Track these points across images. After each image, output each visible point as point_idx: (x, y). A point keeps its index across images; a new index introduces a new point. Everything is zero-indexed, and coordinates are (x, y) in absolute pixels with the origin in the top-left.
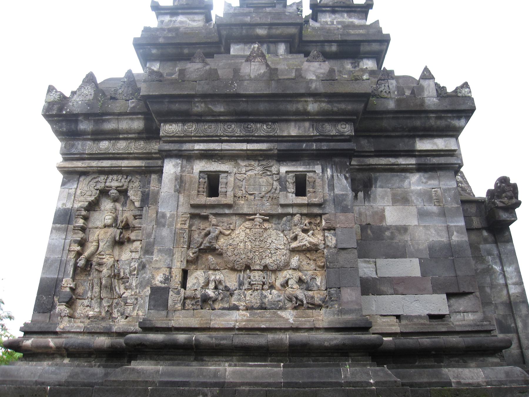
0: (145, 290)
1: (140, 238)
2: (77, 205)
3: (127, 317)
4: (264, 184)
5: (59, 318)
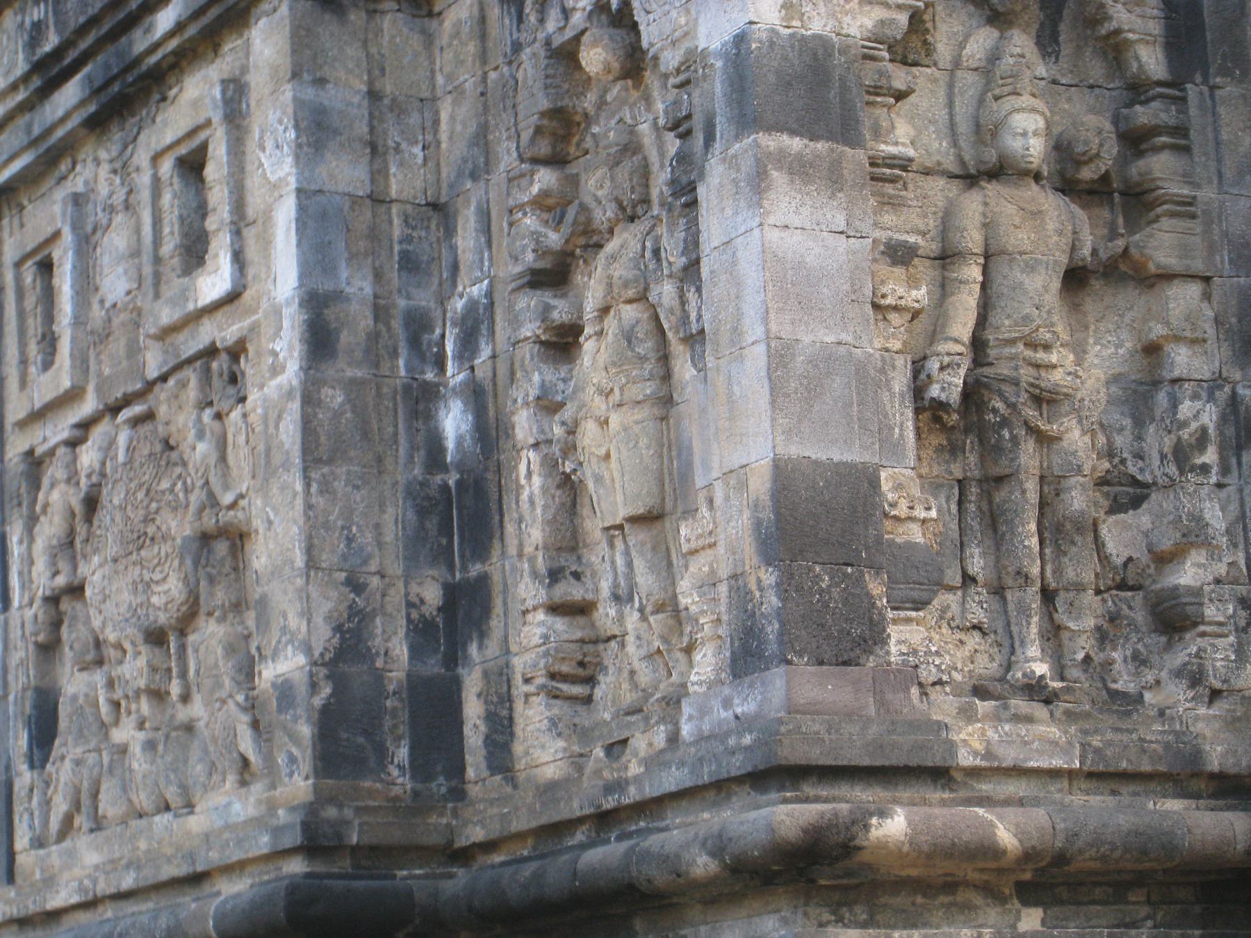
1: (1198, 266)
3: (1215, 694)
5: (915, 691)
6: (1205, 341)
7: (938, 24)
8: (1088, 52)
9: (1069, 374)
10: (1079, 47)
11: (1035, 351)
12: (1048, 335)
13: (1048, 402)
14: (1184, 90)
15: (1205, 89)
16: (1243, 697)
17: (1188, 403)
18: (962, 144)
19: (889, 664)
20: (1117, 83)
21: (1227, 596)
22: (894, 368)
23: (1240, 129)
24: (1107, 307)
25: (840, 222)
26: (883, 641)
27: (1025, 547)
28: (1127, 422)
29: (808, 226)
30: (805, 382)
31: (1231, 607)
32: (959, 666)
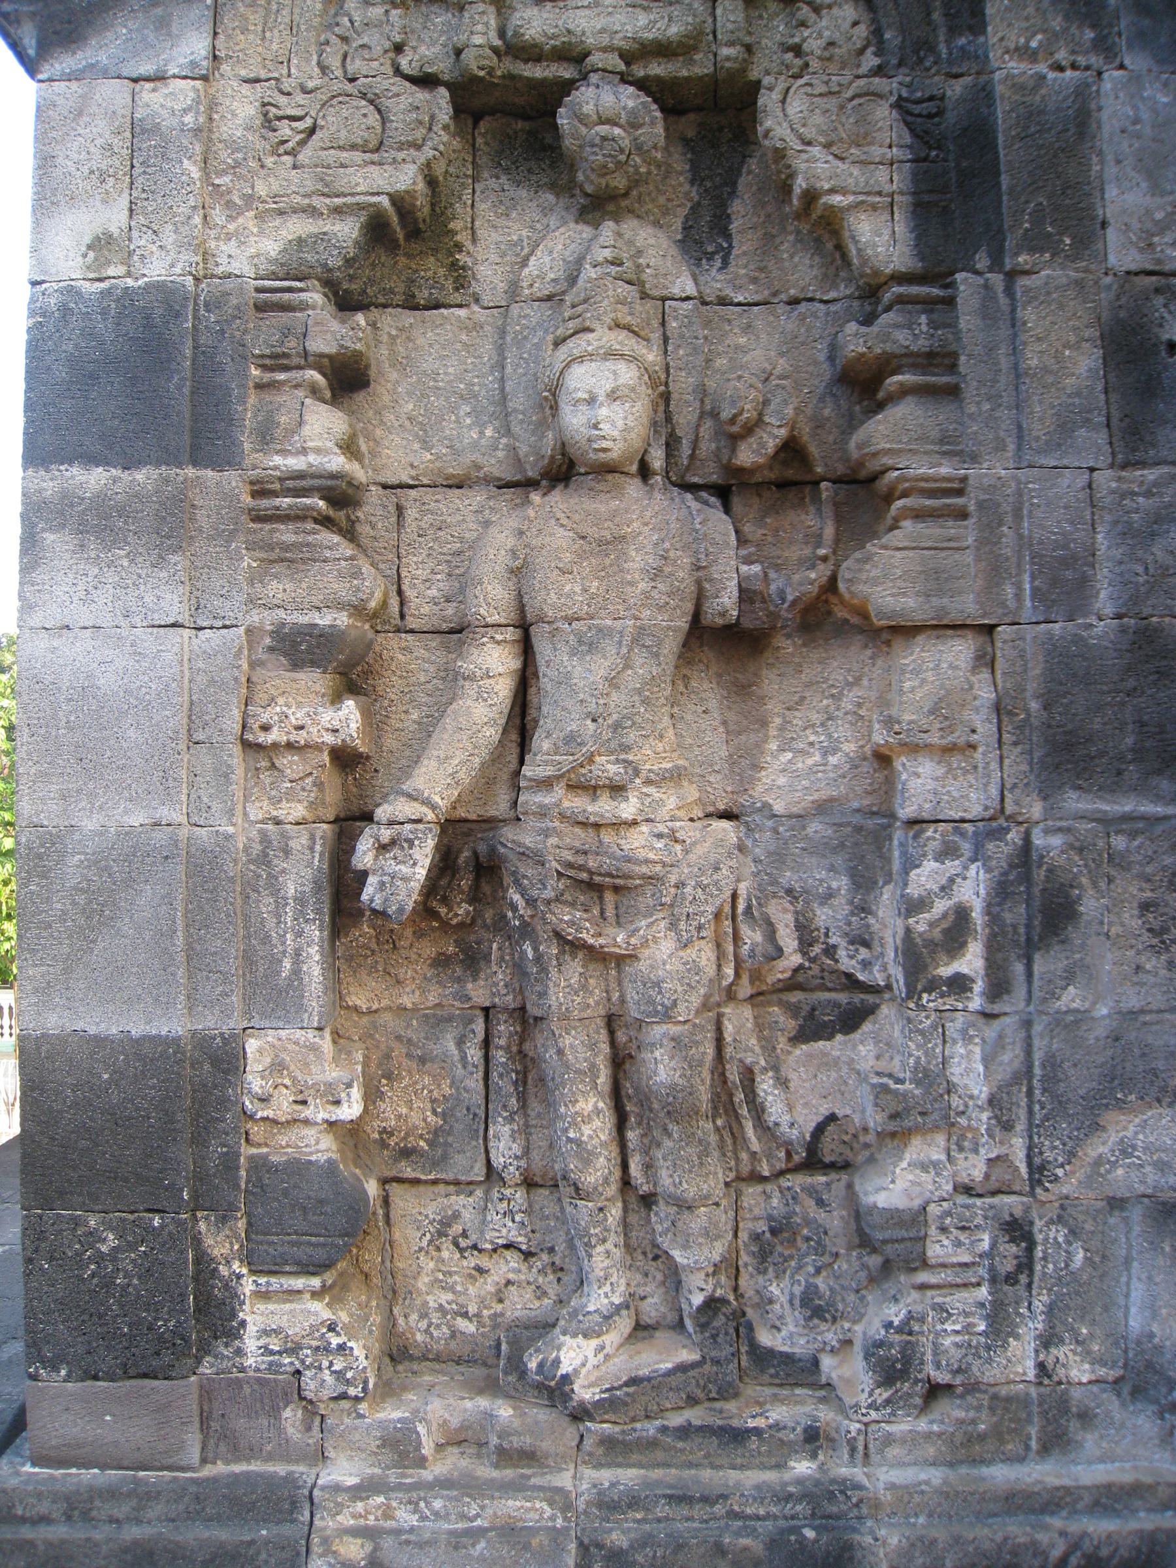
0: (1099, 1147)
1: (967, 606)
2: (249, 251)
3: (934, 1391)
5: (291, 1415)
6: (973, 747)
7: (480, 233)
8: (787, 244)
9: (660, 836)
10: (769, 237)
11: (594, 798)
12: (613, 769)
13: (616, 889)
14: (952, 285)
15: (997, 280)
16: (995, 1397)
17: (930, 865)
18: (516, 429)
19: (242, 1370)
20: (844, 290)
22: (287, 852)
23: (1066, 346)
24: (809, 685)
25: (173, 605)
26: (232, 1331)
27: (569, 1140)
28: (841, 883)
29: (106, 621)
30: (81, 899)
31: (986, 1237)
32: (472, 1309)
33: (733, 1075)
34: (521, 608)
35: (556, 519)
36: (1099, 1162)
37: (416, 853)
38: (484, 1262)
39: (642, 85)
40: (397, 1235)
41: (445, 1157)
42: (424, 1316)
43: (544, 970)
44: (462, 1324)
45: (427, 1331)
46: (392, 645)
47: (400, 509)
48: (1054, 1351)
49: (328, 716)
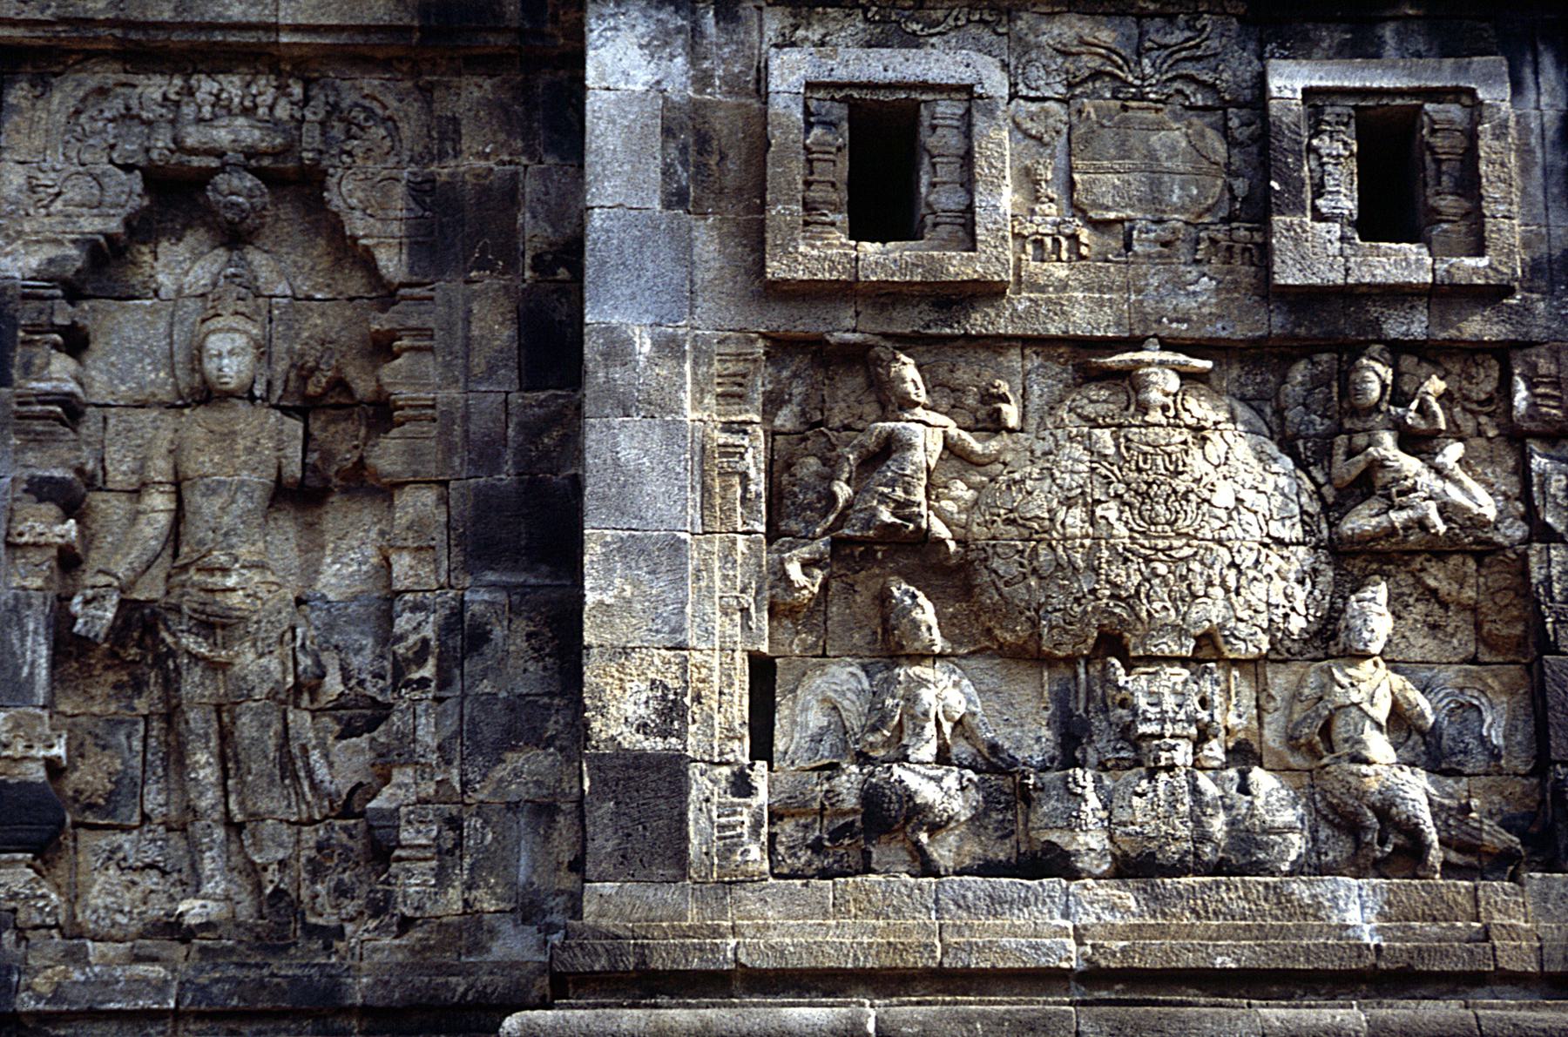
0: (499, 772)
1: (431, 470)
3: (406, 924)
4: (1177, 164)
5: (9, 937)
12: (223, 558)
13: (224, 627)
18: (178, 373)
21: (431, 817)
22: (30, 606)
23: (496, 322)
28: (368, 642)
32: (127, 909)
33: (295, 749)
34: (176, 473)
35: (198, 424)
36: (501, 780)
37: (107, 604)
38: (137, 878)
39: (257, 172)
40: (81, 859)
41: (115, 809)
42: (95, 911)
43: (180, 674)
44: (120, 918)
45: (96, 922)
46: (96, 498)
47: (105, 419)
48: (474, 893)
49: (58, 529)
